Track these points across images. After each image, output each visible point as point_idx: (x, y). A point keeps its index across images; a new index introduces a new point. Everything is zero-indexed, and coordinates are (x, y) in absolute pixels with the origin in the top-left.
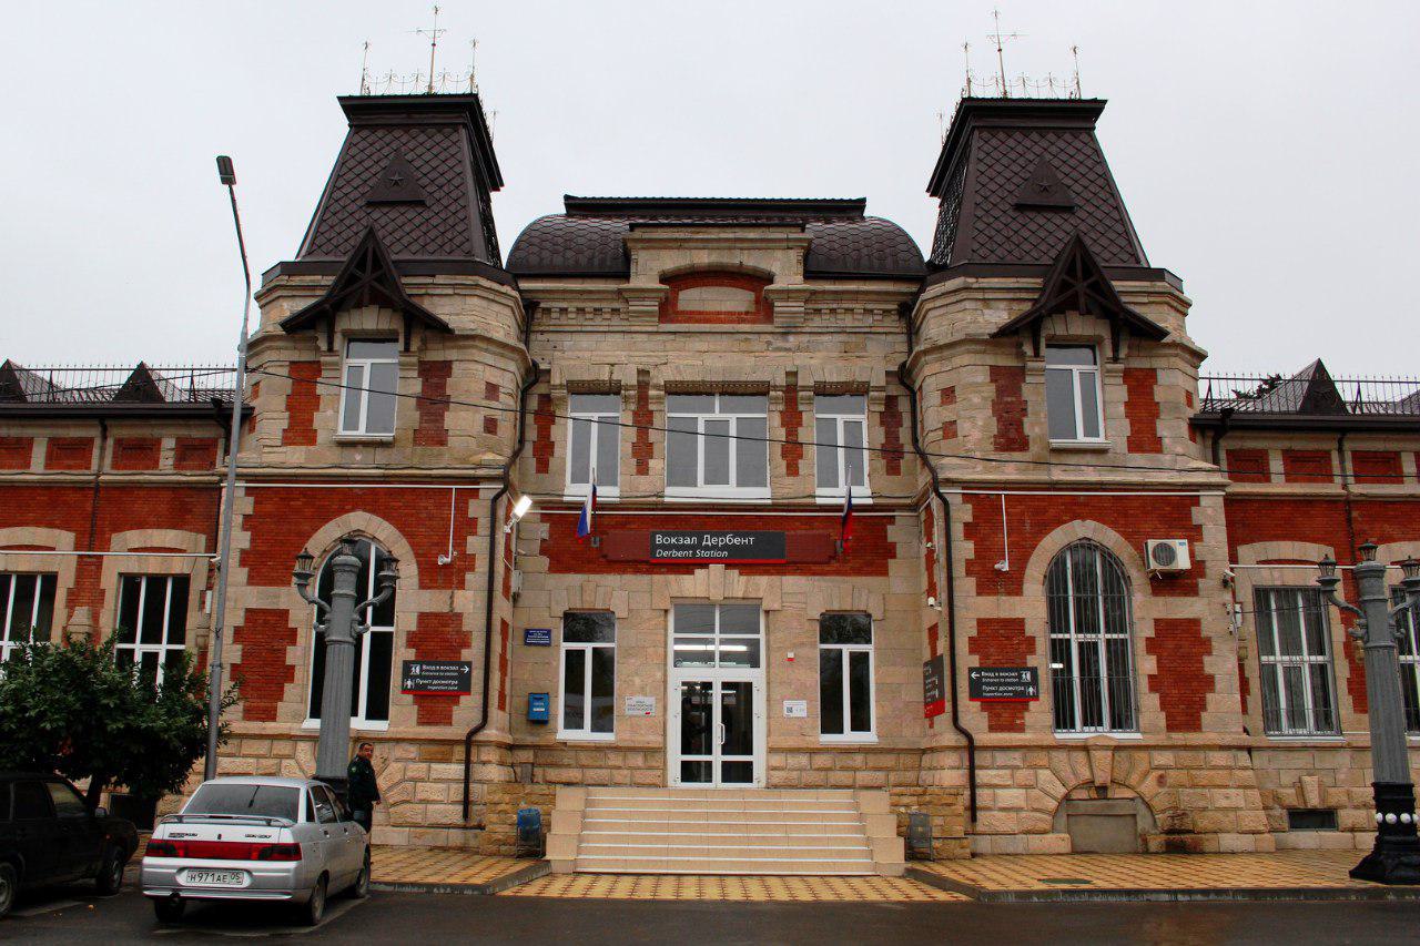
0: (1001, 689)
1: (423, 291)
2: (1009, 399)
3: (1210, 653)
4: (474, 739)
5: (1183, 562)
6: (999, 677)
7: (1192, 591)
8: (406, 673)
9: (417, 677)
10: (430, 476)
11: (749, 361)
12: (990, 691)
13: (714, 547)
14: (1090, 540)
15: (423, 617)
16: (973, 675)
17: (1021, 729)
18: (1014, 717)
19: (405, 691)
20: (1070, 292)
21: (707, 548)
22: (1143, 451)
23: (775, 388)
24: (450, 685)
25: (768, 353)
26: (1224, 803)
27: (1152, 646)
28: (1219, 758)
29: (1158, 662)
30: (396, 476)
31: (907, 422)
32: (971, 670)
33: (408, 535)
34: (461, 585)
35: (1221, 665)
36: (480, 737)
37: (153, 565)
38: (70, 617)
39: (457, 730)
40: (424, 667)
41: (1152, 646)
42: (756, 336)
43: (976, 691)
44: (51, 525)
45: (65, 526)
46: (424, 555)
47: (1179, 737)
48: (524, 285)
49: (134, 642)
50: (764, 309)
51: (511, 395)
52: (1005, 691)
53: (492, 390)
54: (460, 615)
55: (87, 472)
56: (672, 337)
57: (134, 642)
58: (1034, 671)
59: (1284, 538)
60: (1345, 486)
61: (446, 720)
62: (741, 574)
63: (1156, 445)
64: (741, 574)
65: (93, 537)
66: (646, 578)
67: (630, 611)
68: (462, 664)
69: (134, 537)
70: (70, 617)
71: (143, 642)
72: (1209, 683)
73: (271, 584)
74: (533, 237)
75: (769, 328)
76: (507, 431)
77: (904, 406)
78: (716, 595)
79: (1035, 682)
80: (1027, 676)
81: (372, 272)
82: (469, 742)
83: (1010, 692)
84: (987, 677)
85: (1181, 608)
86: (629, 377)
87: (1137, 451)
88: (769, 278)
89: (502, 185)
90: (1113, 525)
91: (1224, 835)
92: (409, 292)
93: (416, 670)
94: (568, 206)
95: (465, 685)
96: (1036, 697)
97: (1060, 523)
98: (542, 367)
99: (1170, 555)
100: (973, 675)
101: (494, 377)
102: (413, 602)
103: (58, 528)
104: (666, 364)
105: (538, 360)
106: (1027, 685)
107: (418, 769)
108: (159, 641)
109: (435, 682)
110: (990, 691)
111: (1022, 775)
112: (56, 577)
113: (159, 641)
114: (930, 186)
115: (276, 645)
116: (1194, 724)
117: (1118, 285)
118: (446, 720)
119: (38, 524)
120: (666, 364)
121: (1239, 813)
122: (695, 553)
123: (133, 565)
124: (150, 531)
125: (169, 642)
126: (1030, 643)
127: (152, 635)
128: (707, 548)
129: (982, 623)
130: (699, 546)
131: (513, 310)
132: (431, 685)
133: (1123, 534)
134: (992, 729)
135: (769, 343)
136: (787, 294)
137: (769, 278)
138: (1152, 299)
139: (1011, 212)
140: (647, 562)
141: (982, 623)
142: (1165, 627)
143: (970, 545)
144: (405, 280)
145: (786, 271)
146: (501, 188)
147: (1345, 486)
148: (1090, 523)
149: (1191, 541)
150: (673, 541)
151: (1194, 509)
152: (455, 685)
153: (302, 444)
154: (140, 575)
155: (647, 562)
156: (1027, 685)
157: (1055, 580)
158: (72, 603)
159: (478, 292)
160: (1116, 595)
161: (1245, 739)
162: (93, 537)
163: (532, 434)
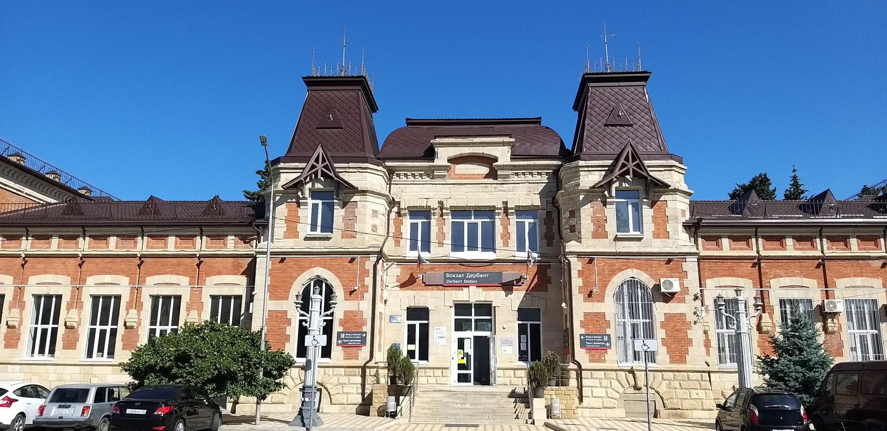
0: (594, 344)
1: (344, 170)
2: (599, 215)
3: (690, 329)
4: (367, 365)
5: (676, 288)
6: (593, 338)
7: (683, 301)
8: (339, 338)
9: (343, 339)
10: (349, 252)
11: (487, 195)
12: (589, 345)
13: (471, 279)
14: (634, 278)
15: (346, 313)
16: (582, 337)
17: (604, 361)
18: (600, 356)
19: (338, 344)
20: (625, 169)
21: (468, 279)
22: (660, 238)
23: (498, 209)
24: (357, 342)
25: (494, 193)
26: (696, 396)
27: (663, 325)
28: (693, 376)
29: (666, 332)
30: (333, 252)
31: (556, 222)
32: (581, 335)
33: (340, 277)
34: (362, 298)
35: (695, 334)
36: (369, 365)
37: (226, 291)
38: (128, 313)
39: (361, 362)
40: (346, 334)
41: (663, 325)
42: (490, 185)
43: (583, 345)
44: (177, 274)
45: (185, 274)
46: (346, 286)
47: (675, 367)
48: (387, 164)
49: (96, 325)
50: (493, 174)
51: (383, 215)
52: (596, 345)
53: (375, 213)
54: (362, 312)
55: (194, 250)
56: (453, 185)
57: (96, 325)
58: (609, 336)
59: (729, 276)
60: (758, 252)
61: (356, 357)
62: (483, 290)
63: (667, 235)
64: (483, 290)
65: (198, 280)
66: (443, 292)
67: (436, 307)
68: (363, 333)
69: (216, 279)
70: (128, 313)
71: (42, 324)
72: (690, 342)
73: (279, 300)
74: (394, 137)
75: (495, 181)
76: (382, 230)
77: (555, 216)
78: (473, 301)
79: (609, 341)
80: (606, 338)
81: (322, 164)
82: (364, 368)
83: (598, 345)
84: (588, 338)
85: (672, 308)
86: (434, 204)
87: (657, 238)
88: (496, 160)
89: (378, 110)
90: (646, 271)
91: (695, 411)
92: (337, 170)
93: (343, 336)
94: (408, 124)
95: (364, 343)
96: (610, 347)
97: (621, 270)
98: (396, 200)
99: (671, 284)
100: (582, 337)
101: (375, 207)
102: (342, 306)
103: (181, 275)
104: (450, 198)
105: (395, 197)
106: (606, 342)
107: (345, 379)
108: (167, 325)
109: (351, 341)
110: (589, 345)
111: (605, 383)
112: (475, 336)
113: (167, 325)
114: (574, 106)
115: (282, 326)
116: (683, 360)
117: (647, 163)
118: (356, 357)
119: (171, 273)
120: (450, 198)
121: (702, 400)
122: (463, 281)
123: (216, 292)
124: (224, 276)
125: (172, 325)
126: (608, 324)
127: (164, 322)
128: (468, 279)
129: (586, 314)
130: (465, 278)
131: (383, 177)
132: (349, 342)
133: (650, 275)
134: (590, 361)
135: (495, 188)
136: (504, 167)
137: (496, 160)
138: (666, 169)
139: (603, 127)
140: (442, 285)
141: (586, 314)
142: (669, 317)
143: (581, 280)
144: (336, 165)
145: (503, 155)
146: (378, 111)
147: (758, 252)
148: (635, 270)
149: (681, 278)
150: (454, 276)
151: (684, 264)
152: (359, 342)
153: (292, 238)
154: (219, 296)
155: (442, 285)
156: (606, 342)
157: (619, 296)
158: (188, 309)
159: (368, 170)
160: (637, 302)
161: (706, 368)
162: (198, 280)
163: (392, 229)
